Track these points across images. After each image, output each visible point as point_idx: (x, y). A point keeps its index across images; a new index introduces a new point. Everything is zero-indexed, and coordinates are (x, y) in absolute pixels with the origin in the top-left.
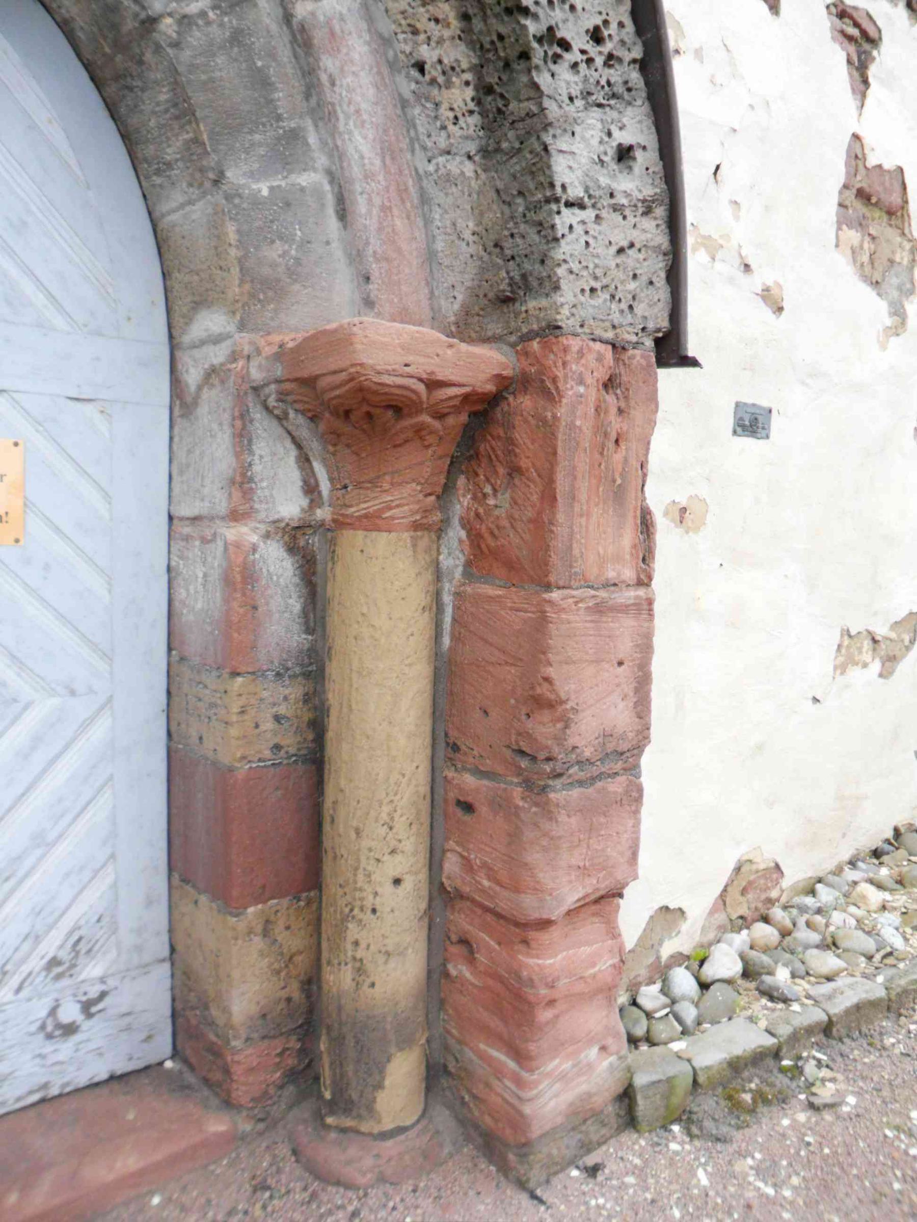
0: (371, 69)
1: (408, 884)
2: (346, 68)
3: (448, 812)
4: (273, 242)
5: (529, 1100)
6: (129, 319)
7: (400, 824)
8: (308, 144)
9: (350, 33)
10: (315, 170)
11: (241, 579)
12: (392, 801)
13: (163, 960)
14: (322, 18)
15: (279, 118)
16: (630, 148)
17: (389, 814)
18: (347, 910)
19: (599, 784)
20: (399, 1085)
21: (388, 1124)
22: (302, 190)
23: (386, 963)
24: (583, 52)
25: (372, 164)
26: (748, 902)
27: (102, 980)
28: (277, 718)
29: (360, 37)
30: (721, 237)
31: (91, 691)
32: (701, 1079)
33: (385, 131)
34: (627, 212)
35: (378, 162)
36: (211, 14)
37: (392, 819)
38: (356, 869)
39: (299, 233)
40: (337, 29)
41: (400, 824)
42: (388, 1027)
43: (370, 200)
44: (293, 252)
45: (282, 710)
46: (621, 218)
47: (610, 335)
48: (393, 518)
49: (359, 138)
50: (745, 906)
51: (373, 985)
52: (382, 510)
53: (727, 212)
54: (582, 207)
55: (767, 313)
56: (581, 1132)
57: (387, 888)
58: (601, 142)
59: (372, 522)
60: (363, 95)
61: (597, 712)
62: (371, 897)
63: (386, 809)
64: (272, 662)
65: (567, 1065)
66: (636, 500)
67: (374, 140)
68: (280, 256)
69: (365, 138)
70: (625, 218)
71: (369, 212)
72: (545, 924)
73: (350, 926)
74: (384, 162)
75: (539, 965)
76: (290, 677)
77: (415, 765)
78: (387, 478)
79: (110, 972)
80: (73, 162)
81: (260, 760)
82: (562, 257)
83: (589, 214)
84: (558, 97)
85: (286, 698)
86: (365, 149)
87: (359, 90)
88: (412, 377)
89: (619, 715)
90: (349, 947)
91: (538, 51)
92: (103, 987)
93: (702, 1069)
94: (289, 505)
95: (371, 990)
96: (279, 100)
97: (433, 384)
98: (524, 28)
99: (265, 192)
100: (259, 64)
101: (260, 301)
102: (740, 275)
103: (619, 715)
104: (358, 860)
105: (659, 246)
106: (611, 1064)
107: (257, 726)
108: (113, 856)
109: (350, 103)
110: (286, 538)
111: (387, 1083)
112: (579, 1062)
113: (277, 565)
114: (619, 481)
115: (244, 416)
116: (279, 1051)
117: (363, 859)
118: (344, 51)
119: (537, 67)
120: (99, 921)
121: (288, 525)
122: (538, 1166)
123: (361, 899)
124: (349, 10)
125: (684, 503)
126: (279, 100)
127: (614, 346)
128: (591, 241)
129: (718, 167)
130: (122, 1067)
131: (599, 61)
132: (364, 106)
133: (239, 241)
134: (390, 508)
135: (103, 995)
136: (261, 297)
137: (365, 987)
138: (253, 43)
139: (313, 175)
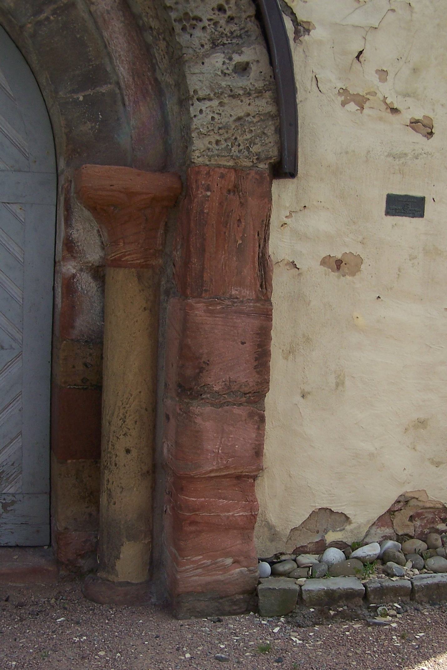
0: (125, 35)
1: (134, 453)
2: (112, 36)
3: (153, 420)
4: (85, 123)
5: (180, 572)
6: (35, 162)
7: (129, 421)
8: (106, 71)
9: (113, 19)
10: (110, 83)
11: (70, 287)
12: (125, 408)
13: (46, 493)
14: (99, 13)
15: (90, 60)
16: (248, 63)
17: (123, 414)
18: (106, 464)
19: (226, 408)
20: (128, 562)
21: (121, 579)
22: (103, 94)
23: (121, 492)
24: (210, 20)
25: (128, 81)
26: (415, 527)
27: (13, 495)
28: (85, 365)
29: (118, 20)
30: (367, 94)
31: (11, 348)
32: (305, 596)
33: (134, 64)
34: (243, 98)
35: (131, 80)
36: (52, 18)
37: (125, 417)
38: (108, 442)
39: (100, 116)
40: (106, 18)
41: (129, 421)
42: (122, 527)
43: (129, 98)
44: (97, 127)
45: (89, 360)
46: (239, 101)
47: (231, 163)
48: (127, 261)
49: (122, 69)
50: (412, 529)
51: (115, 504)
52: (121, 257)
53: (374, 79)
54: (210, 99)
55: (419, 138)
56: (219, 603)
57: (122, 453)
58: (224, 63)
59: (117, 263)
60: (121, 48)
61: (227, 366)
62: (114, 457)
63: (122, 411)
64: (83, 336)
65: (209, 562)
66: (254, 252)
67: (128, 69)
68: (89, 129)
69: (124, 68)
70: (242, 101)
71: (129, 104)
72: (192, 479)
73: (106, 471)
74: (134, 79)
75: (186, 499)
76: (93, 343)
77: (138, 390)
78: (122, 241)
79: (18, 492)
80: (8, 88)
81: (75, 385)
82: (195, 127)
83: (215, 103)
84: (193, 46)
85: (90, 355)
86: (125, 74)
87: (119, 46)
88: (115, 191)
89: (244, 376)
90: (105, 483)
91: (178, 27)
92: (13, 499)
93: (305, 590)
94: (94, 255)
95: (114, 506)
96: (90, 51)
97: (130, 194)
98: (170, 17)
99: (81, 98)
100: (78, 36)
101: (78, 153)
102: (389, 116)
103: (244, 376)
104: (109, 437)
105: (269, 113)
106: (241, 571)
107: (74, 367)
108: (21, 433)
109: (116, 52)
110: (92, 271)
111: (121, 556)
112: (216, 563)
113: (86, 283)
114: (240, 242)
115: (68, 209)
116: (84, 540)
117: (111, 437)
118: (111, 28)
119: (178, 34)
120: (13, 464)
121: (93, 265)
122: (185, 609)
123: (110, 458)
124: (112, 7)
125: (339, 256)
126: (90, 51)
127: (236, 171)
128: (216, 116)
129: (361, 52)
130: (21, 542)
131: (222, 22)
132: (122, 53)
133: (66, 125)
134: (125, 256)
135: (13, 502)
136: (79, 150)
137: (111, 504)
138: (75, 27)
139: (109, 86)
